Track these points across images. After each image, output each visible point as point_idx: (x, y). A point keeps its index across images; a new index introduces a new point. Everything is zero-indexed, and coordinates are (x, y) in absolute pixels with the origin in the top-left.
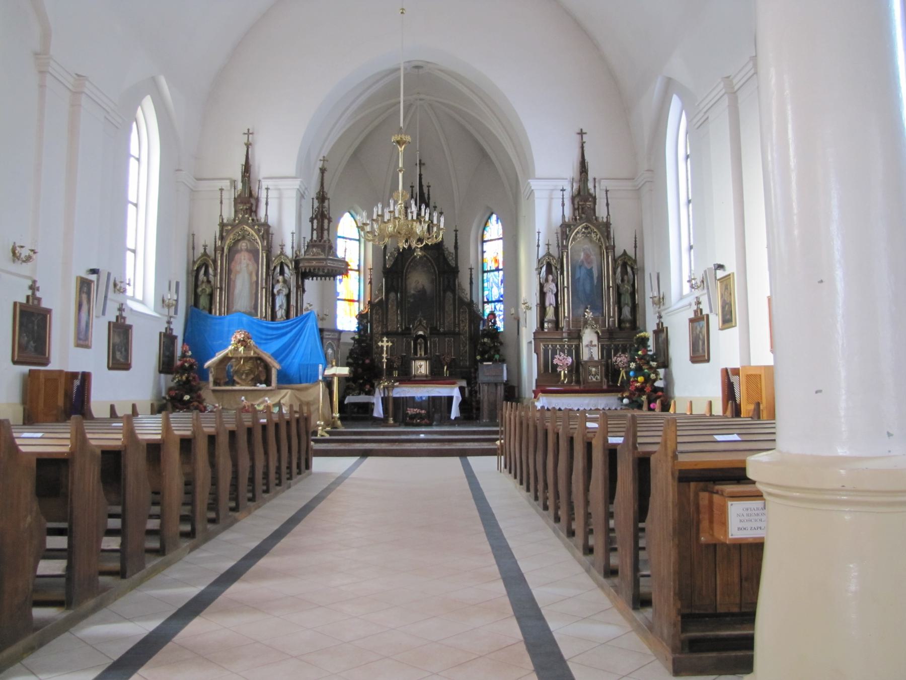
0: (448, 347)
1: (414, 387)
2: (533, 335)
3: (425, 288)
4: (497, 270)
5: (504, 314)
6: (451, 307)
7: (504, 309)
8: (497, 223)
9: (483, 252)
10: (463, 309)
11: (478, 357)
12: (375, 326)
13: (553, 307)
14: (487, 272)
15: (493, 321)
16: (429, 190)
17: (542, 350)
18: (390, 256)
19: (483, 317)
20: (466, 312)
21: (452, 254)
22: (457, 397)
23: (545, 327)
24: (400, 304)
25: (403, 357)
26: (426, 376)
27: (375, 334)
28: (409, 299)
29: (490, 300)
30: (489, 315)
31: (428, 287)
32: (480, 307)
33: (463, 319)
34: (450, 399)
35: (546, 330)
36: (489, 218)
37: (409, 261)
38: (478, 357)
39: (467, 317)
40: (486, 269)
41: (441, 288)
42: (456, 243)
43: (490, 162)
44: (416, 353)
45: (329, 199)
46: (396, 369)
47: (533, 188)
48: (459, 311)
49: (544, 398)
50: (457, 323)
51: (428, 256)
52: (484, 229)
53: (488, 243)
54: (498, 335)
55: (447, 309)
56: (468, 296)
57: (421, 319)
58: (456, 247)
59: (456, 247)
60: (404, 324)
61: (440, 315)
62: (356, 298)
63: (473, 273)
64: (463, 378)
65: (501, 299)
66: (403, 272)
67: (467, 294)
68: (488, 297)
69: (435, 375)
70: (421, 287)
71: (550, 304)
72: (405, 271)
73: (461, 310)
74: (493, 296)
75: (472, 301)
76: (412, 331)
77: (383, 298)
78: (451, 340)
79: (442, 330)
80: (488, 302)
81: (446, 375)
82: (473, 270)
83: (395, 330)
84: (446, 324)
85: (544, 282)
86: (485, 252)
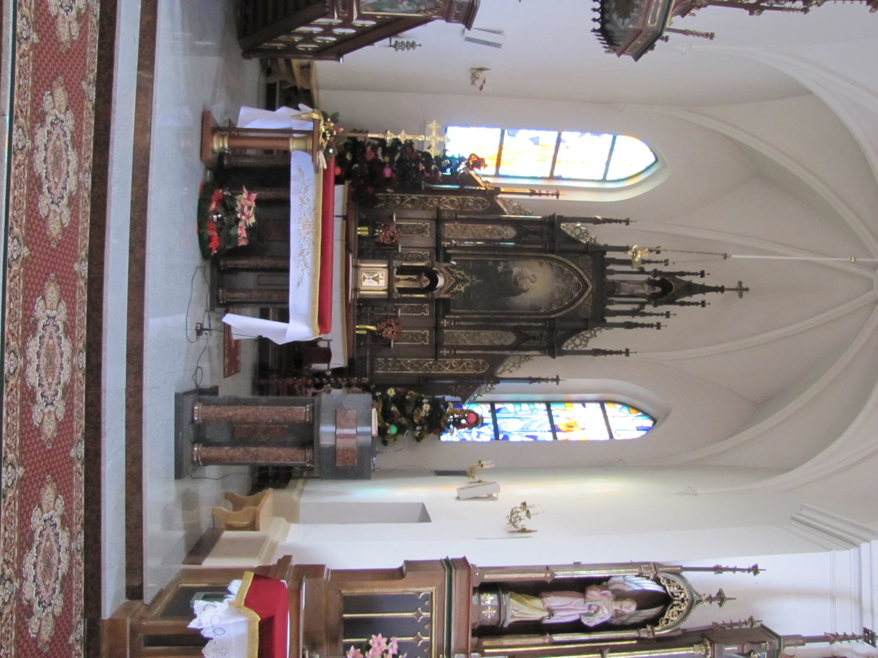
0: (412, 333)
1: (316, 215)
2: (459, 556)
3: (523, 294)
4: (554, 429)
5: (473, 442)
6: (486, 342)
7: (483, 443)
8: (639, 429)
9: (583, 402)
10: (484, 364)
11: (391, 392)
12: (454, 198)
13: (543, 618)
14: (549, 410)
15: (463, 421)
16: (697, 304)
17: (412, 590)
18: (581, 230)
19: (467, 401)
20: (478, 369)
21: (585, 346)
22: (284, 332)
23: (483, 597)
24: (492, 248)
25: (395, 246)
26: (356, 290)
27: (439, 198)
28: (501, 263)
29: (498, 415)
30: (476, 415)
31: (524, 300)
32: (486, 397)
33: (465, 364)
34: (284, 316)
35: (474, 599)
36: (645, 414)
37: (573, 265)
38: (391, 392)
39: (469, 372)
40: (553, 407)
41: (524, 324)
42: (605, 353)
43: (748, 422)
44: (402, 271)
45: (805, 10)
46: (372, 232)
47: (864, 546)
48: (479, 356)
49: (243, 630)
50: (457, 352)
51: (581, 301)
52: (624, 404)
53: (600, 411)
54: (435, 433)
55: (483, 333)
56: (506, 375)
57: (468, 281)
58: (597, 352)
59: (597, 352)
60: (457, 252)
61: (474, 320)
62: (502, 172)
63: (550, 383)
64: (351, 361)
65: (501, 437)
66: (553, 252)
67: (511, 372)
68: (502, 411)
69: (359, 307)
70: (525, 287)
71: (551, 613)
72: (554, 256)
73: (481, 361)
74: (505, 420)
75: (497, 381)
76: (446, 265)
77: (505, 214)
78: (425, 340)
79: (445, 323)
80: (493, 411)
81: (358, 329)
82: (555, 383)
83: (446, 236)
84: (456, 332)
85: (613, 587)
86: (584, 406)
